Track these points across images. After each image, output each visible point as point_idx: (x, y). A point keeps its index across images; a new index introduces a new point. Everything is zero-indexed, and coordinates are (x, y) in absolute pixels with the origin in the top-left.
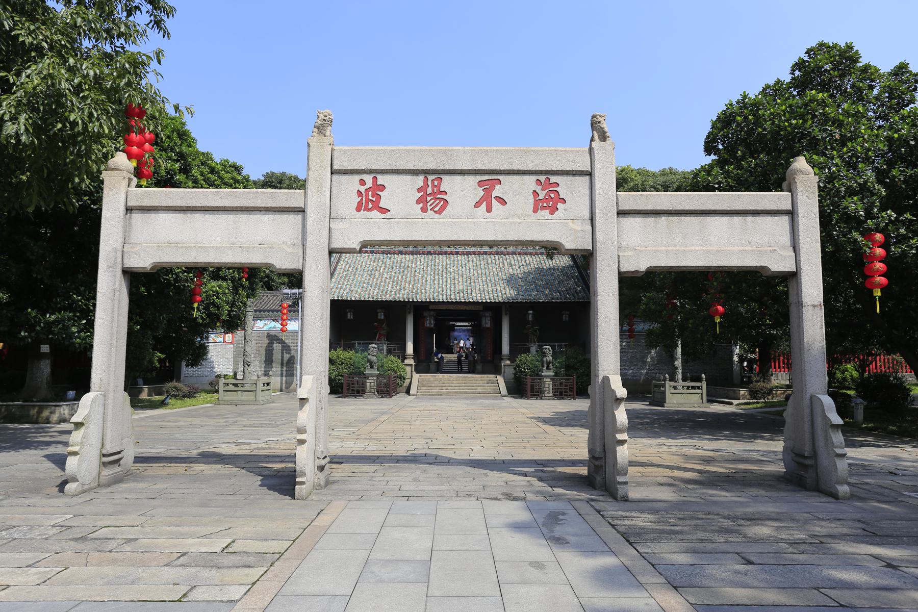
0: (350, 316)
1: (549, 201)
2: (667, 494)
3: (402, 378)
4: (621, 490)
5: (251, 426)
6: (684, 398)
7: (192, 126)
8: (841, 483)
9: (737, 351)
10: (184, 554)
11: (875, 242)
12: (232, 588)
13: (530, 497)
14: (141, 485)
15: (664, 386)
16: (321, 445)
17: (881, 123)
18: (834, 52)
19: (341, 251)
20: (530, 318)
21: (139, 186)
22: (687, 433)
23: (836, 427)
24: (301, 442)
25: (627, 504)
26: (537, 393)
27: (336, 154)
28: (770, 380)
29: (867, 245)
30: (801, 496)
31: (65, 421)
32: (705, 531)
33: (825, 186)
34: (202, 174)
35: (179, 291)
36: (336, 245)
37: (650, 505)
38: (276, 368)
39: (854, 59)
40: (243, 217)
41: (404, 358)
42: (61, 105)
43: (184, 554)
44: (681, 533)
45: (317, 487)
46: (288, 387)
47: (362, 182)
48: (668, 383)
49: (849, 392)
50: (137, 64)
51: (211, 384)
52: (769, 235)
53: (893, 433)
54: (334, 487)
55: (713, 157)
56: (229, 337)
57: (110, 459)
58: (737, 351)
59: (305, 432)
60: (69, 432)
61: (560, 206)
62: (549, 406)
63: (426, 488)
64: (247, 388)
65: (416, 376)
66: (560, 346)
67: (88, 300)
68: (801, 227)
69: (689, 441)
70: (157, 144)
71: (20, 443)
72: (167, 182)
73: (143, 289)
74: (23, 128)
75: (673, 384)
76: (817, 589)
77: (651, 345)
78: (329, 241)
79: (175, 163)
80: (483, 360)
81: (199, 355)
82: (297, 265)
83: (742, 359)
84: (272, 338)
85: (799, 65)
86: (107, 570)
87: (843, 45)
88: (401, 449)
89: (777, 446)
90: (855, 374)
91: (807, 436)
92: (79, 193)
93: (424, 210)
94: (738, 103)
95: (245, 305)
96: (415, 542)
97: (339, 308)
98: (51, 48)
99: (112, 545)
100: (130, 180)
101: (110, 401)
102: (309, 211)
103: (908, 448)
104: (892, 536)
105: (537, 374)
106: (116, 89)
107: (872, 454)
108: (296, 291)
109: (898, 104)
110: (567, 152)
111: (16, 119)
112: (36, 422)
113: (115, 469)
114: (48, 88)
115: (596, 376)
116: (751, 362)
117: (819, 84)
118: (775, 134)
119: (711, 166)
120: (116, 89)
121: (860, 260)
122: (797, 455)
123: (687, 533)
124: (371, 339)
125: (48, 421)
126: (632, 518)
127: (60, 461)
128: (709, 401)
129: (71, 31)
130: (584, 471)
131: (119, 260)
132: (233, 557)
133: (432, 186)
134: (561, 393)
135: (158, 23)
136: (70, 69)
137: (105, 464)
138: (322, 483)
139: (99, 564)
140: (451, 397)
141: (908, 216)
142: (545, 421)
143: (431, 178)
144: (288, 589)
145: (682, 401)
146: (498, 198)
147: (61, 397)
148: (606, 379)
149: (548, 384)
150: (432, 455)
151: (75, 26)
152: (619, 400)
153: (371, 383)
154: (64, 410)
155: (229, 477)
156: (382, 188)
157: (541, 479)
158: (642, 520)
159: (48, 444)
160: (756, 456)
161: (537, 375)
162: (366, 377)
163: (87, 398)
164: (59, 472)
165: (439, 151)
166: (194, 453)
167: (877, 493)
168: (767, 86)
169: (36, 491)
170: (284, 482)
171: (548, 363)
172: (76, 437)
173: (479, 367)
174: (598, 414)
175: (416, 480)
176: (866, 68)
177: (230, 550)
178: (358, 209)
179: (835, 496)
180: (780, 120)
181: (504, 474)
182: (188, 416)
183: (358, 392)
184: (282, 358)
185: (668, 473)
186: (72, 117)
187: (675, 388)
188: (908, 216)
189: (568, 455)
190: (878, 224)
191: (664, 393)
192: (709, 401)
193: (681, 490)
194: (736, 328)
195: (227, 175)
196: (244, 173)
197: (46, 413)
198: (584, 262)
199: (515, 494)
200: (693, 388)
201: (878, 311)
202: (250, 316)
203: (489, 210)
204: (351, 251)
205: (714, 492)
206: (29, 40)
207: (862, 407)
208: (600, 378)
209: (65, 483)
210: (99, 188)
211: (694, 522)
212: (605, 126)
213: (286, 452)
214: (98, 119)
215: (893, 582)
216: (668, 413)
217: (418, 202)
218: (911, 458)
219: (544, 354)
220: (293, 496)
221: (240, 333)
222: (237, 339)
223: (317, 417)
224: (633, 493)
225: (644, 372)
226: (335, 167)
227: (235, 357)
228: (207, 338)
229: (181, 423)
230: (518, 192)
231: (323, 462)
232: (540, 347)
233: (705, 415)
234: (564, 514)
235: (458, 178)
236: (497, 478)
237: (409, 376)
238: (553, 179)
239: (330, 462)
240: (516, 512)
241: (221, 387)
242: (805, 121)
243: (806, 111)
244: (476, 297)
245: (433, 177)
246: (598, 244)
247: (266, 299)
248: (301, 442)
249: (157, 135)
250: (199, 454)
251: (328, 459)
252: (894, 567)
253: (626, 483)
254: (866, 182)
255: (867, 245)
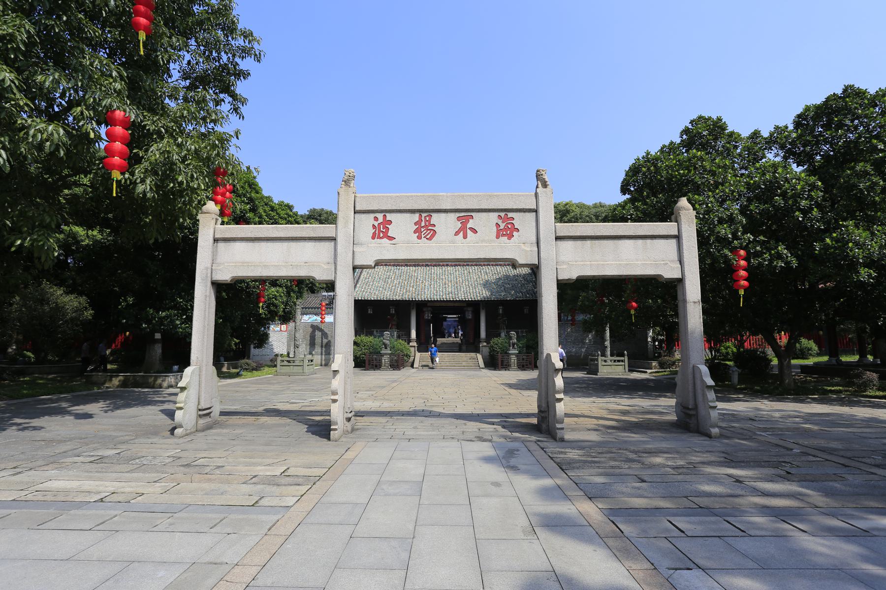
0: (370, 311)
1: (507, 231)
2: (594, 437)
3: (408, 356)
4: (559, 434)
5: (300, 390)
6: (612, 368)
7: (261, 181)
8: (713, 427)
9: (651, 334)
10: (255, 476)
11: (740, 257)
12: (287, 498)
13: (495, 439)
14: (225, 431)
15: (597, 360)
16: (349, 403)
17: (743, 171)
18: (710, 122)
19: (362, 267)
20: (501, 311)
21: (223, 223)
22: (612, 394)
23: (710, 387)
24: (335, 401)
25: (563, 443)
26: (506, 366)
27: (357, 200)
28: (674, 355)
29: (734, 259)
30: (685, 436)
31: (171, 386)
32: (616, 461)
33: (704, 217)
34: (265, 211)
35: (249, 294)
36: (357, 263)
37: (579, 444)
38: (318, 349)
39: (723, 128)
40: (293, 244)
41: (409, 341)
42: (172, 170)
43: (255, 476)
44: (599, 462)
45: (346, 433)
46: (327, 364)
47: (376, 219)
48: (600, 358)
49: (728, 363)
50: (224, 140)
51: (271, 360)
52: (667, 252)
53: (758, 391)
54: (358, 432)
55: (628, 196)
56: (284, 327)
57: (204, 413)
58: (651, 334)
59: (337, 394)
60: (176, 394)
61: (515, 233)
62: (514, 375)
63: (422, 433)
64: (297, 363)
65: (418, 355)
66: (522, 332)
67: (187, 302)
68: (685, 247)
69: (612, 399)
70: (234, 192)
71: (144, 402)
72: (240, 219)
73: (224, 294)
74: (148, 187)
75: (603, 358)
76: (686, 497)
77: (588, 330)
78: (352, 261)
79: (249, 207)
80: (470, 344)
81: (262, 340)
82: (330, 277)
83: (654, 340)
84: (315, 328)
85: (686, 131)
86: (206, 486)
87: (715, 118)
88: (406, 407)
89: (672, 402)
90: (735, 350)
91: (691, 394)
92: (182, 227)
93: (419, 238)
94: (643, 158)
95: (295, 304)
96: (412, 469)
97: (361, 306)
98: (167, 131)
99: (207, 470)
100: (217, 220)
101: (204, 372)
102: (339, 239)
103: (766, 402)
104: (743, 462)
105: (506, 353)
106: (209, 158)
107: (741, 406)
108: (332, 294)
109: (754, 159)
110: (520, 196)
111: (144, 181)
112: (153, 387)
113: (207, 420)
114: (165, 159)
115: (542, 353)
116: (661, 342)
117: (700, 144)
118: (669, 180)
119: (626, 202)
120: (209, 158)
121: (731, 270)
122: (684, 408)
123: (603, 462)
124: (386, 328)
125: (161, 387)
126: (565, 453)
127: (171, 414)
128: (629, 371)
129: (178, 120)
130: (534, 421)
131: (209, 275)
132: (288, 479)
133: (424, 221)
134: (523, 366)
135: (236, 110)
136: (179, 146)
137: (200, 416)
138: (350, 430)
139: (200, 482)
140: (443, 369)
141: (762, 238)
142: (510, 386)
143: (424, 215)
144: (324, 499)
145: (610, 371)
146: (472, 229)
147: (168, 370)
148: (549, 355)
149: (514, 359)
150: (427, 411)
151: (182, 116)
152: (557, 371)
153: (385, 360)
154: (171, 379)
155: (284, 425)
156: (390, 222)
157: (504, 427)
158: (573, 454)
159: (163, 402)
160: (660, 409)
161: (506, 353)
162: (382, 355)
163: (188, 371)
164: (170, 422)
165: (429, 197)
166: (261, 409)
167: (739, 433)
168: (664, 146)
169: (156, 434)
170: (322, 429)
171: (514, 344)
172: (182, 397)
173: (464, 347)
174: (543, 380)
175: (415, 428)
176: (732, 134)
177: (286, 474)
178: (373, 238)
179: (709, 436)
180: (673, 171)
181: (478, 424)
182: (255, 384)
183: (376, 366)
184: (321, 341)
185: (595, 421)
186: (180, 179)
187: (605, 361)
188: (762, 238)
189: (524, 410)
190: (741, 244)
191: (597, 365)
192: (629, 371)
193: (604, 434)
194: (648, 317)
195: (282, 214)
196: (294, 210)
197: (159, 381)
198: (535, 270)
199: (485, 437)
200: (619, 361)
201: (114, 195)
202: (299, 312)
203: (465, 237)
204: (368, 267)
205: (626, 434)
206: (152, 128)
207: (736, 373)
208: (545, 355)
209: (174, 428)
210: (196, 222)
211: (608, 455)
212: (546, 177)
213: (325, 409)
214: (197, 179)
215: (739, 492)
216: (600, 379)
217: (415, 232)
218: (767, 409)
219: (510, 338)
220: (329, 439)
221: (291, 324)
222: (289, 328)
223: (345, 384)
224: (567, 437)
225: (583, 350)
226: (357, 209)
227: (288, 342)
228: (269, 328)
229: (252, 388)
230: (486, 224)
231: (350, 415)
232: (508, 333)
233: (626, 380)
234: (518, 450)
235: (443, 215)
236: (473, 427)
237: (413, 354)
238: (510, 215)
239: (355, 416)
240: (487, 449)
241: (279, 363)
242: (690, 171)
243: (689, 164)
244: (461, 297)
245: (426, 214)
246: (542, 261)
247: (310, 299)
248: (335, 401)
249: (234, 186)
250: (265, 410)
251: (353, 413)
252: (740, 482)
253: (562, 429)
254: (732, 214)
255: (734, 259)
